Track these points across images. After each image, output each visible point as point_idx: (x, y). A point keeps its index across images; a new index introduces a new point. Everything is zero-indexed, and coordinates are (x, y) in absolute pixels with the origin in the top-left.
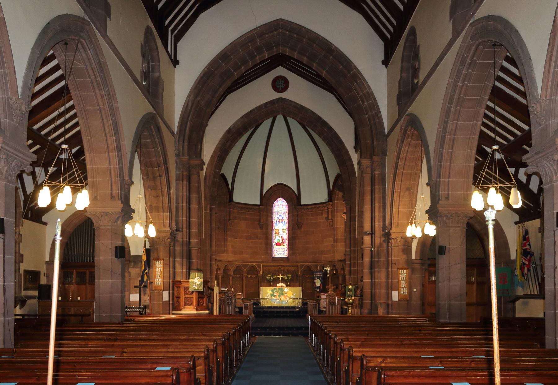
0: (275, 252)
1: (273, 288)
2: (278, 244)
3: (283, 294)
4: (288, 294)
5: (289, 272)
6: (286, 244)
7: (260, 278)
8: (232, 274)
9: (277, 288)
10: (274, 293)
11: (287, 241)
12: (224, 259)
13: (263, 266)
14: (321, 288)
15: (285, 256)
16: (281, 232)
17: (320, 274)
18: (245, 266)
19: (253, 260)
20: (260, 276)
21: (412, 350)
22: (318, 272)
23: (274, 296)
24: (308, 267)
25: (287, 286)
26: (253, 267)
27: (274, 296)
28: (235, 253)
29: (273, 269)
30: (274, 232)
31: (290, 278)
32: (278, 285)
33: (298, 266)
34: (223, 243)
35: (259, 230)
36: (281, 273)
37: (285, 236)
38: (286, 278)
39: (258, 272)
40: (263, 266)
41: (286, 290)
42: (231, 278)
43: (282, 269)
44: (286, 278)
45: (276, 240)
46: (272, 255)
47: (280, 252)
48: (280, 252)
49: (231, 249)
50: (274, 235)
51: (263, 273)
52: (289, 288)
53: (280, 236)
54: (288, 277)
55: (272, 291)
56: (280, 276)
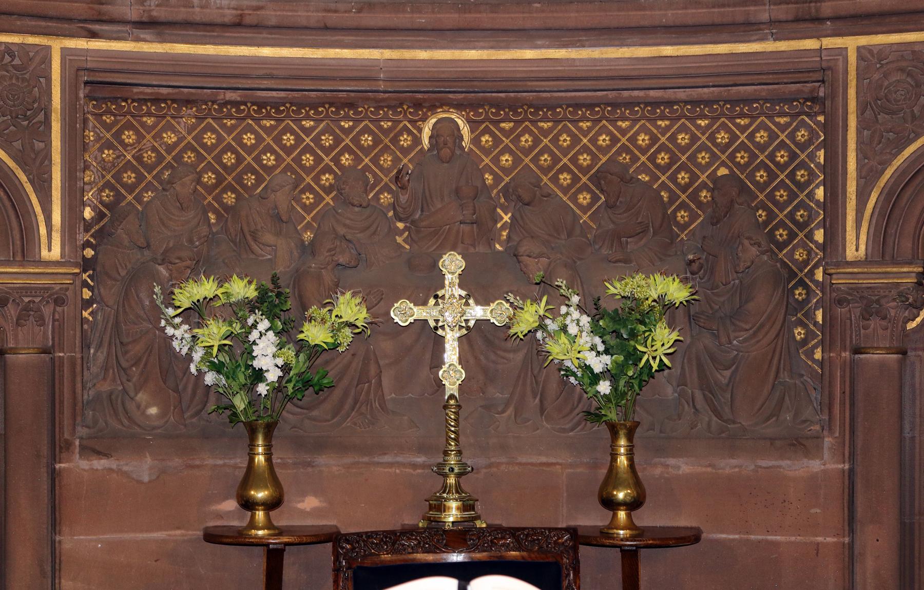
13: (102, 88)
33: (825, 71)
36: (475, 235)
51: (99, 238)
54: (621, 326)
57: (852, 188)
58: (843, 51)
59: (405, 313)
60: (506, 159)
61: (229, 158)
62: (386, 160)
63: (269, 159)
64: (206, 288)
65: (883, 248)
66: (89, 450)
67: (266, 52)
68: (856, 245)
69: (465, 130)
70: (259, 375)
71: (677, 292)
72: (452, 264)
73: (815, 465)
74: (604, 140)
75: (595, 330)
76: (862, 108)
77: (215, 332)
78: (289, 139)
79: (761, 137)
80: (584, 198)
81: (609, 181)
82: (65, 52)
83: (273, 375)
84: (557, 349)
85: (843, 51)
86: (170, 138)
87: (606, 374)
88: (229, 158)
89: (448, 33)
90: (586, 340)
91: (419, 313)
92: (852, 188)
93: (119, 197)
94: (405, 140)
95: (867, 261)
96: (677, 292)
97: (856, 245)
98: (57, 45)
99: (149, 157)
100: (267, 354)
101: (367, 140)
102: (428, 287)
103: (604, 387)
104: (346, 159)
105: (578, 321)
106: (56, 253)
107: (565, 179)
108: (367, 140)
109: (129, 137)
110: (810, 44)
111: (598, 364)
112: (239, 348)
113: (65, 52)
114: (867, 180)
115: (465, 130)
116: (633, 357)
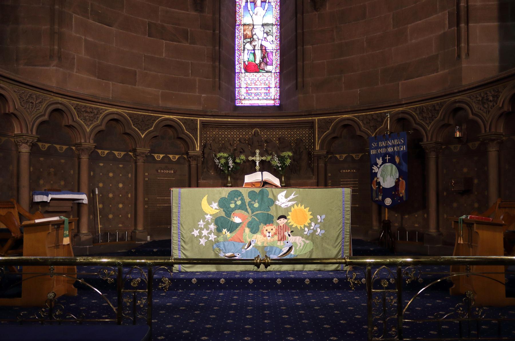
0: (243, 91)
1: (225, 192)
2: (250, 68)
3: (268, 220)
4: (292, 220)
5: (283, 145)
6: (274, 67)
7: (193, 164)
8: (90, 143)
9: (244, 191)
10: (229, 212)
11: (275, 58)
12: (53, 84)
13: (204, 125)
14: (402, 192)
15: (271, 103)
16: (259, 32)
17: (398, 145)
18: (143, 123)
19: (170, 105)
20: (195, 158)
21: (104, 114)
22: (386, 138)
23: (232, 227)
24: (347, 126)
25: (286, 185)
26: (170, 126)
27: (232, 227)
28: (102, 73)
29: (236, 135)
30: (239, 32)
31: (288, 162)
32: (248, 179)
33: (312, 123)
34: (45, 27)
35: (193, 13)
36: (260, 147)
37: (272, 44)
38: (276, 162)
39: (188, 144)
40: (204, 125)
41: (283, 199)
42: (85, 158)
43: (264, 135)
44: (276, 162)
45: (244, 57)
46: (232, 97)
47: (258, 88)
48: (258, 88)
49: (83, 54)
50: (239, 41)
51: (204, 147)
52: (294, 193)
53: (257, 44)
54: (282, 159)
55: (223, 203)
56: (258, 159)
57: (317, 139)
58: (315, 120)
59: (250, 158)
60: (265, 136)
61: (223, 136)
62: (247, 136)
63: (229, 136)
64: (222, 154)
65: (321, 148)
66: (203, 179)
67: (221, 119)
68: (317, 148)
69: (259, 132)
70: (229, 167)
71: (290, 154)
72: (258, 151)
73: (312, 181)
74: (280, 133)
75: (279, 160)
76: (318, 128)
77: (223, 161)
78: (232, 133)
79: (304, 132)
80: (277, 142)
81: (281, 140)
82: (200, 120)
83: (232, 167)
84: (273, 163)
85: (315, 120)
86: (214, 133)
87: (280, 167)
88: (223, 136)
89: (55, 91)
90: (277, 161)
91: (253, 158)
92: (317, 139)
93: (207, 142)
94: (250, 133)
95: (319, 150)
96: (290, 154)
97: (317, 148)
98: (199, 119)
99: (211, 136)
100: (231, 163)
101: (244, 133)
102: (254, 154)
103: (280, 169)
104: (241, 136)
105: (276, 159)
106: (198, 150)
107: (274, 139)
108: (244, 133)
109: (208, 133)
110: (310, 118)
111: (279, 165)
112: (227, 163)
113: (200, 120)
114: (319, 138)
115: (259, 132)
116: (284, 164)
